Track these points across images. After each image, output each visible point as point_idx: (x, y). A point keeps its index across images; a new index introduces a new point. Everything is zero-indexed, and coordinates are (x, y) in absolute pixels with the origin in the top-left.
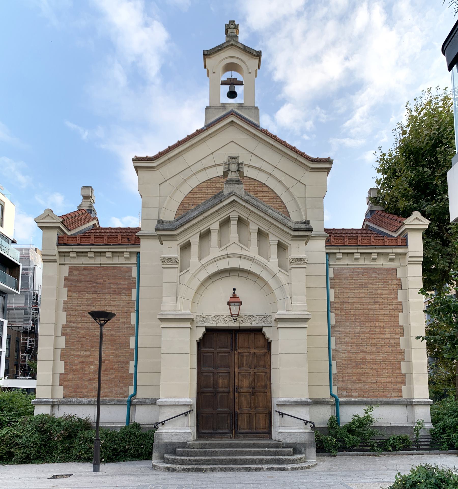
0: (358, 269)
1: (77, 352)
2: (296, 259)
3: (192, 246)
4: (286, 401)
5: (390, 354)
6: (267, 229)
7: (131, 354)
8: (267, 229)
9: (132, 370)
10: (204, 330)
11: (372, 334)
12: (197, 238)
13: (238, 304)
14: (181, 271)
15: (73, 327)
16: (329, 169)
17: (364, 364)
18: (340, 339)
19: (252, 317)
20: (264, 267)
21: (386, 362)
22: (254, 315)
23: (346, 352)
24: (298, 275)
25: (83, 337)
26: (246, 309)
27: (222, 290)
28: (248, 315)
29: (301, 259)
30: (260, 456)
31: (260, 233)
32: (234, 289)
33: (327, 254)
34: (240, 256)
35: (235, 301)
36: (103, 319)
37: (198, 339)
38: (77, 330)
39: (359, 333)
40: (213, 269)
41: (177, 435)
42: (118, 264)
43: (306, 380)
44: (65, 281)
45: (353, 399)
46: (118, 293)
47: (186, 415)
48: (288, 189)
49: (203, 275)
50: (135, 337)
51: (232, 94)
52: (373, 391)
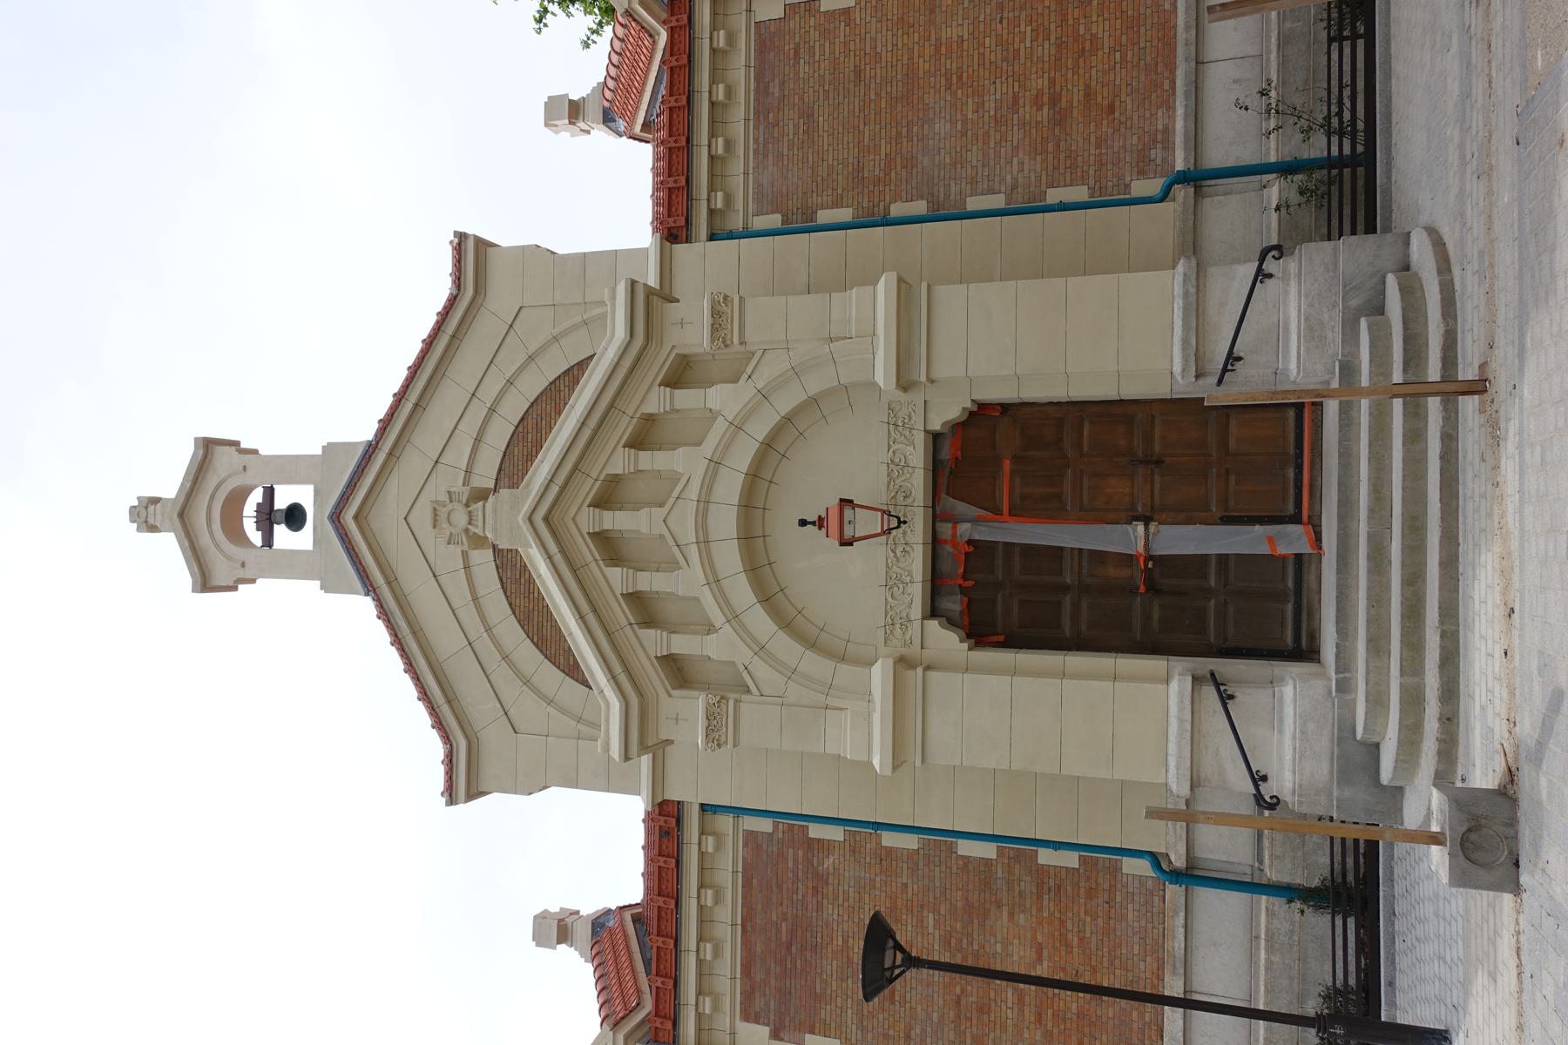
0: (756, 141)
1: (1004, 1028)
2: (715, 328)
3: (673, 651)
4: (1184, 349)
5: (1023, 16)
6: (626, 419)
7: (1019, 857)
8: (626, 419)
9: (1071, 860)
10: (933, 624)
11: (960, 78)
12: (649, 635)
13: (848, 513)
14: (749, 691)
15: (924, 1031)
16: (482, 245)
17: (1054, 101)
18: (973, 182)
19: (896, 466)
20: (737, 427)
21: (1053, 26)
22: (885, 456)
23: (1015, 160)
24: (763, 319)
25: (958, 1003)
26: (868, 486)
27: (811, 563)
28: (885, 479)
29: (716, 313)
30: (1424, 495)
31: (638, 442)
32: (803, 523)
33: (712, 237)
34: (705, 502)
35: (837, 523)
36: (889, 954)
37: (966, 645)
38: (935, 1019)
39: (953, 123)
40: (742, 592)
41: (1303, 733)
42: (735, 872)
43: (1060, 282)
44: (782, 1040)
45: (1179, 125)
46: (820, 881)
47: (1231, 697)
48: (531, 358)
49: (760, 622)
50: (961, 842)
51: (294, 517)
52: (1148, 59)
